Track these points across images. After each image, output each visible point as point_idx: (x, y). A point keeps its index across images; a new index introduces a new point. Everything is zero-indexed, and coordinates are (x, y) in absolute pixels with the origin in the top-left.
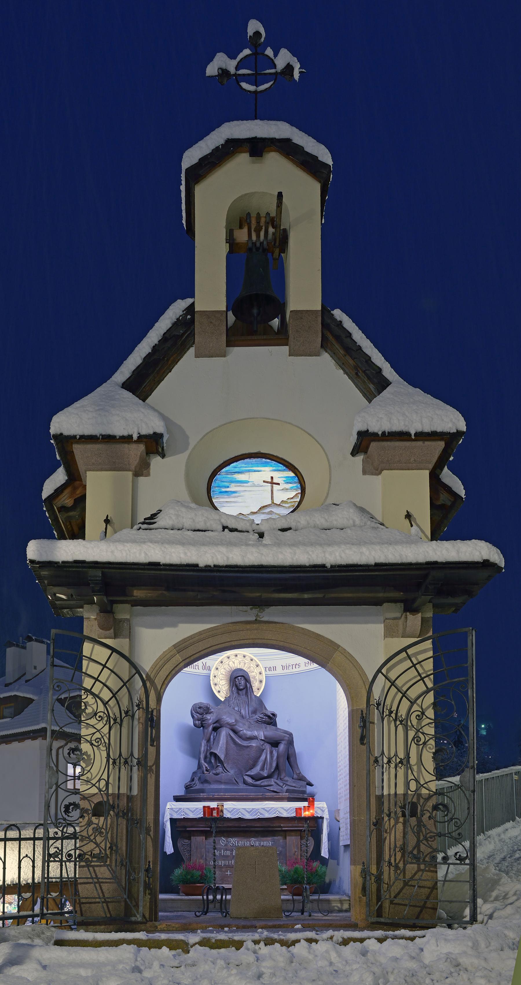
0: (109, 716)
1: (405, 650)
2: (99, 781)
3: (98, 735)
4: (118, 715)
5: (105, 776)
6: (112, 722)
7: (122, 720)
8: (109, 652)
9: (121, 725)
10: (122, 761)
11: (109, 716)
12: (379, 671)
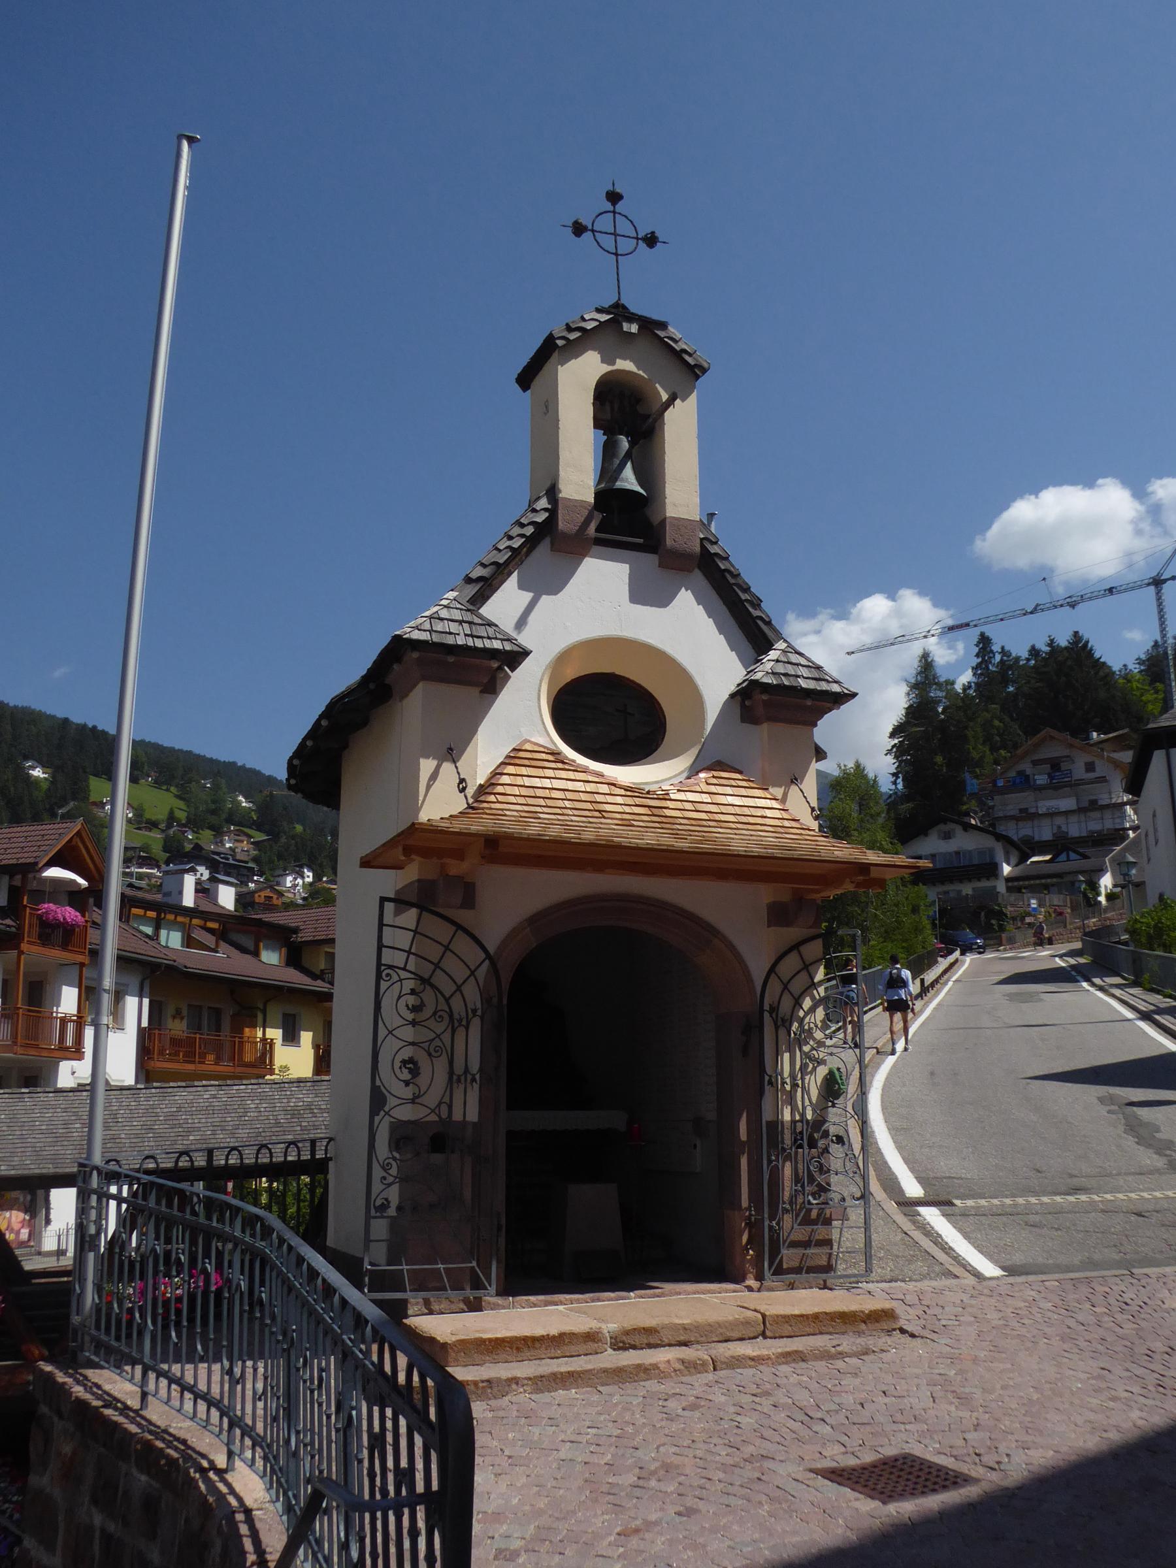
0: (451, 1016)
1: (796, 947)
2: (440, 1103)
3: (437, 1042)
4: (463, 1014)
5: (447, 1099)
6: (456, 1024)
7: (468, 1023)
8: (454, 928)
9: (467, 1028)
10: (469, 1077)
11: (451, 1016)
12: (772, 970)
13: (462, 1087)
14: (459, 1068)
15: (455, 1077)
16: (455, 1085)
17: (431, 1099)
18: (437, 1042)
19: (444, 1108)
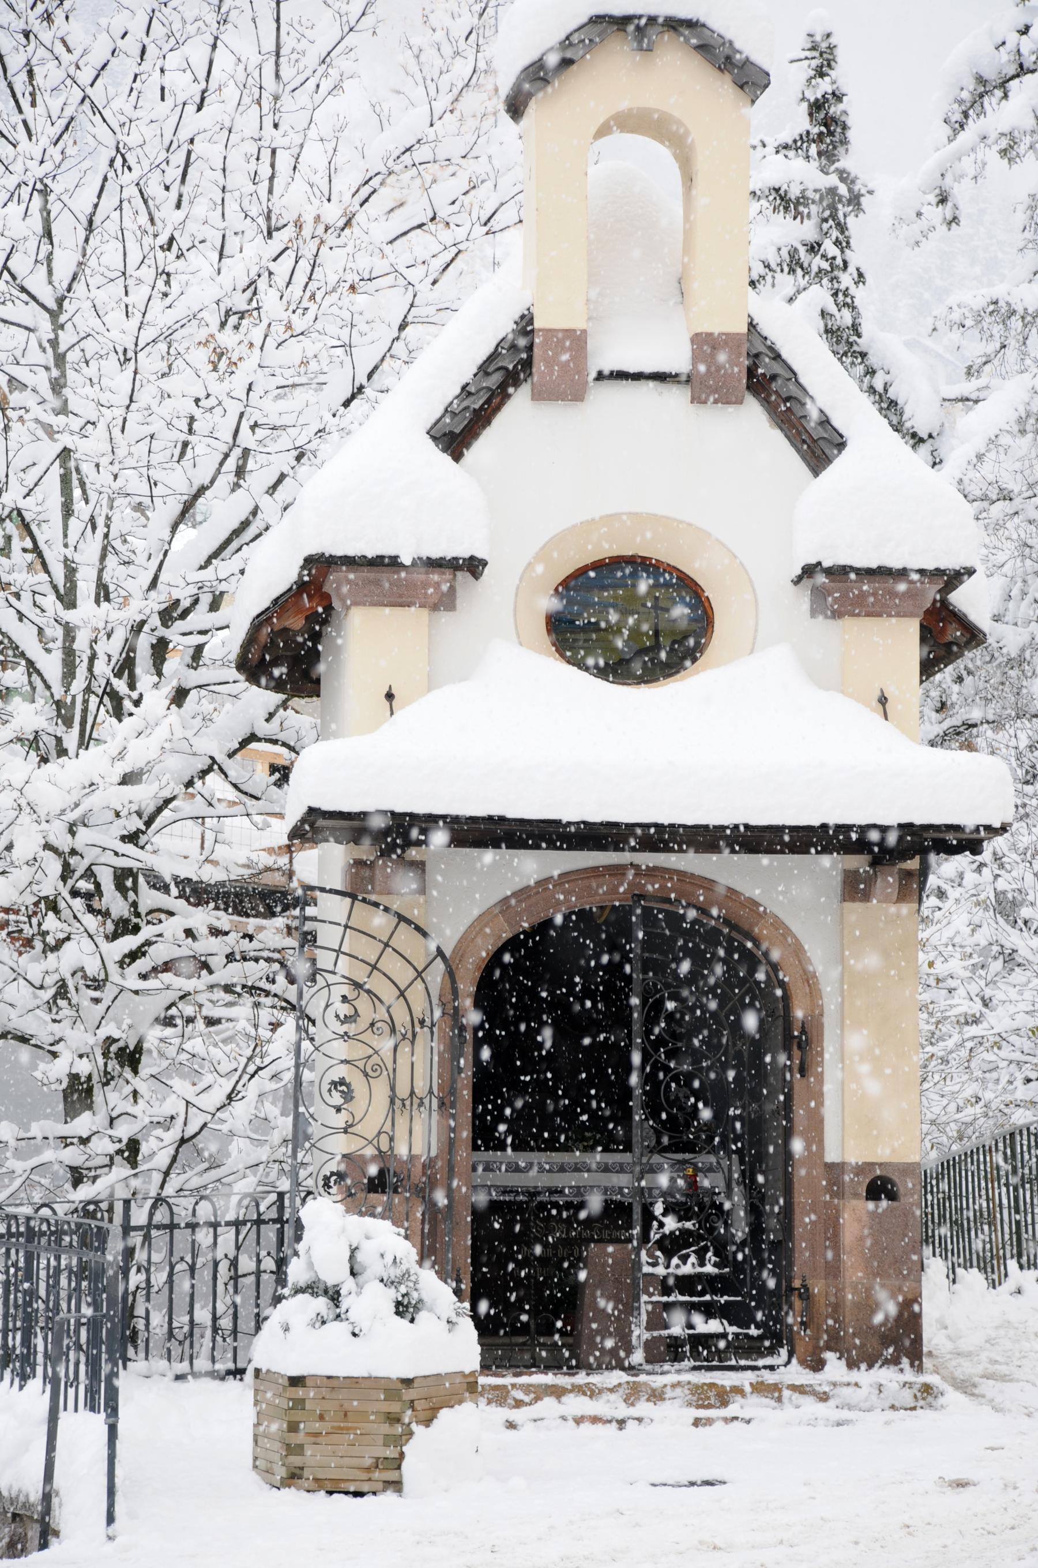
9: (413, 1043)
10: (416, 1101)
13: (407, 1113)
14: (403, 1091)
15: (398, 1103)
16: (398, 1112)
17: (369, 1128)
18: (375, 1059)
19: (384, 1138)
